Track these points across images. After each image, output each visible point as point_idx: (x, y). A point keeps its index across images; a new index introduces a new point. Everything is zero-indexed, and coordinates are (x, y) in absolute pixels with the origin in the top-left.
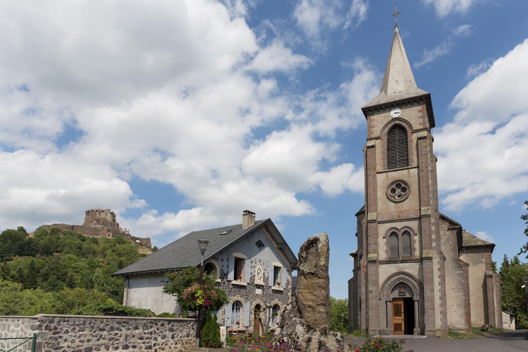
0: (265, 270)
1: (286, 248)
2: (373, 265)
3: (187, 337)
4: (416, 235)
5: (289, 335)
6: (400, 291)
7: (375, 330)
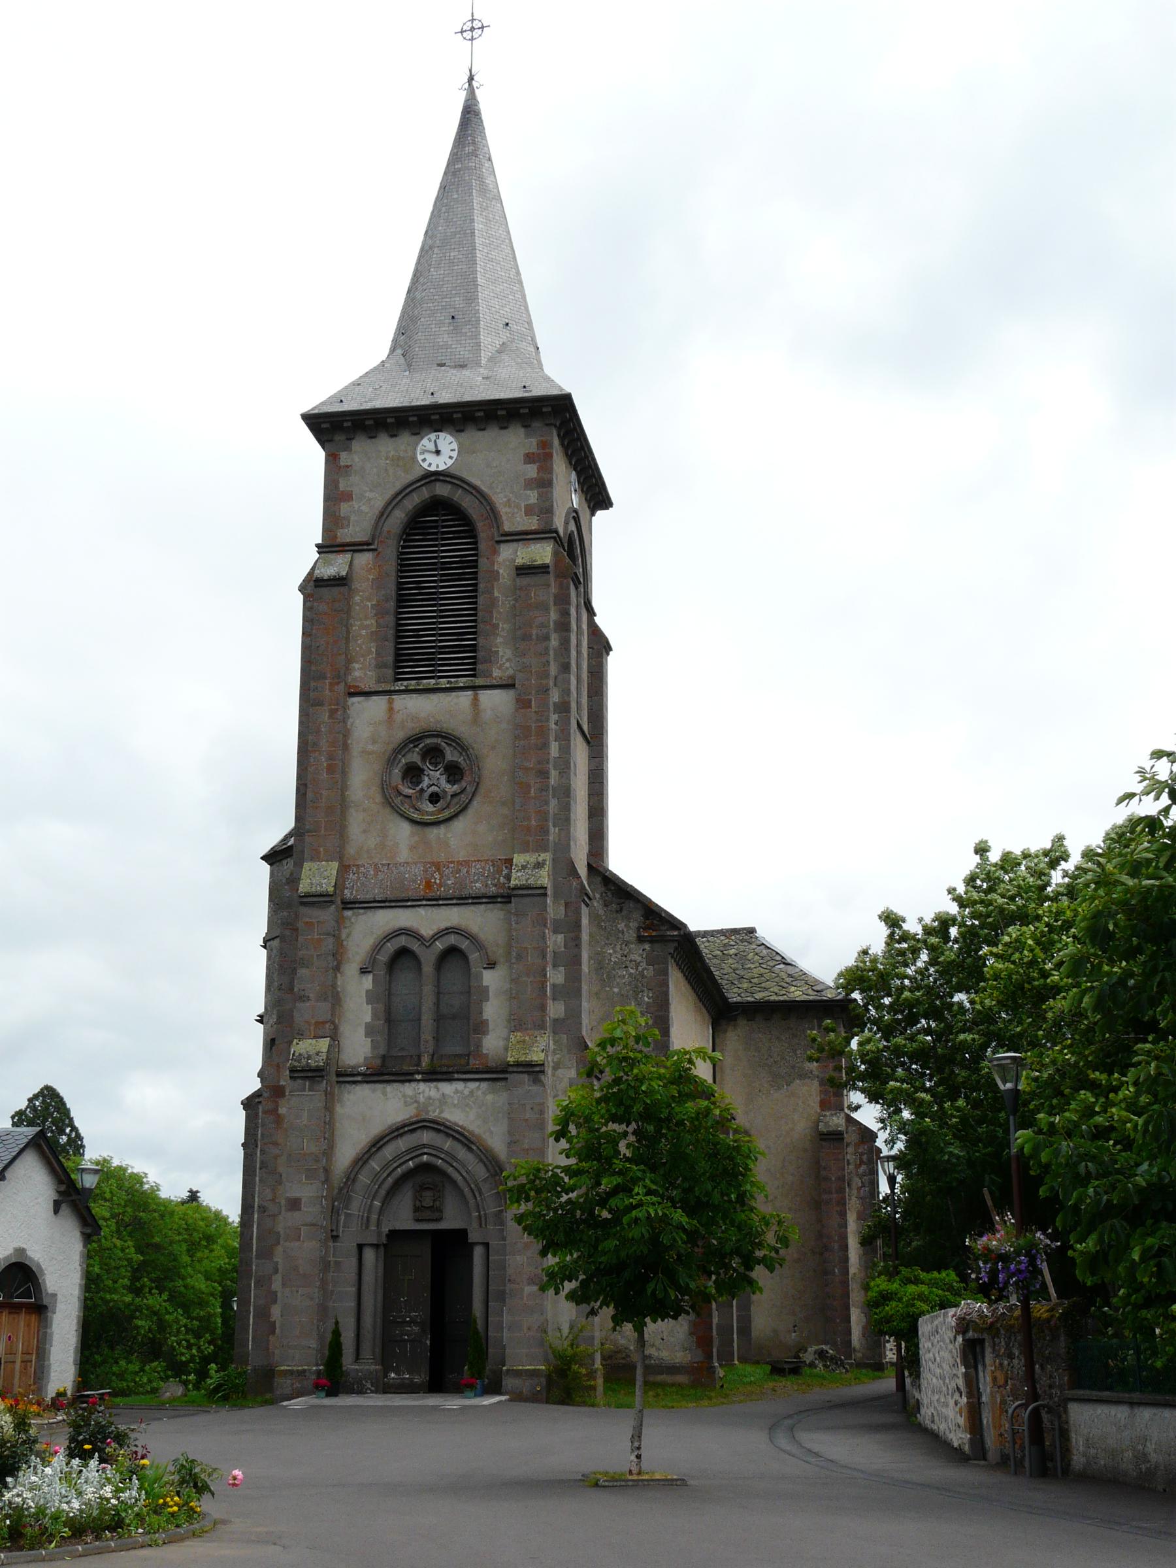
2: (310, 1090)
6: (418, 1203)
7: (305, 1371)
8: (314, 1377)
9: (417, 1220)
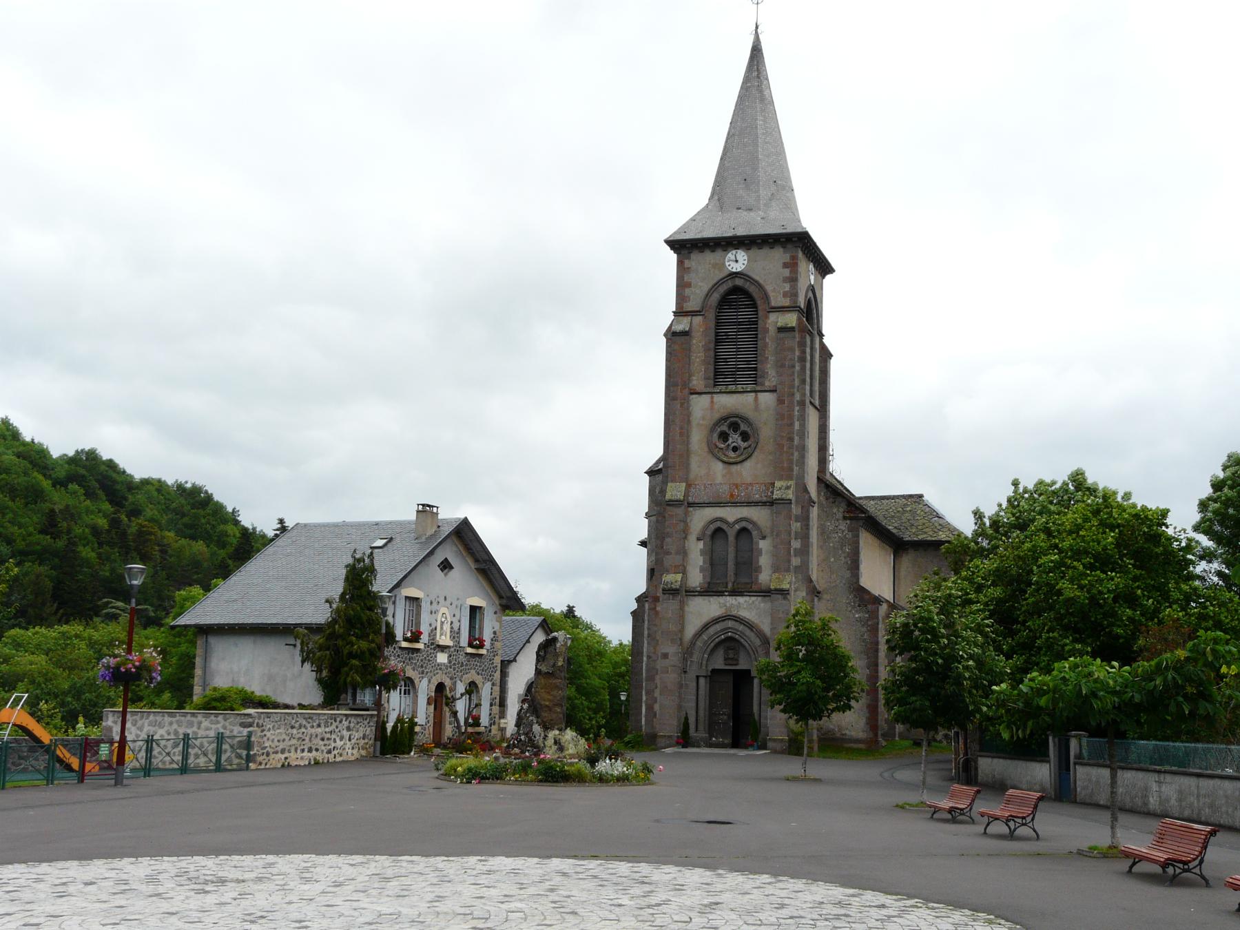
0: (454, 616)
1: (495, 572)
3: (364, 739)
4: (764, 538)
5: (526, 734)
8: (676, 739)
9: (726, 665)
